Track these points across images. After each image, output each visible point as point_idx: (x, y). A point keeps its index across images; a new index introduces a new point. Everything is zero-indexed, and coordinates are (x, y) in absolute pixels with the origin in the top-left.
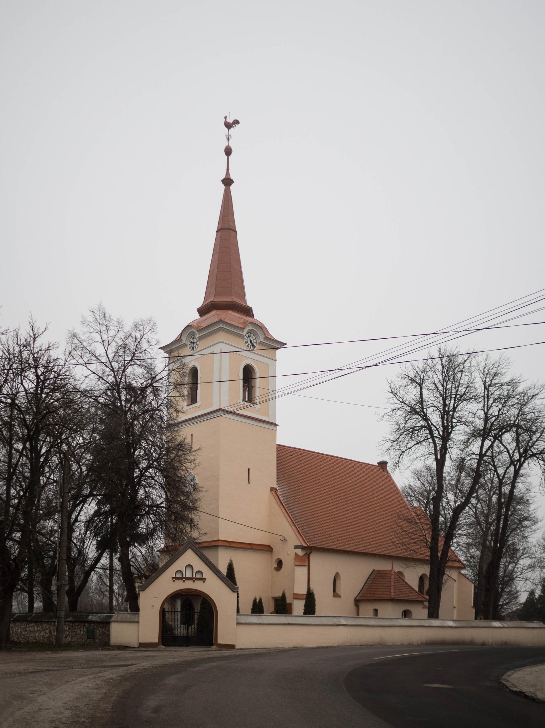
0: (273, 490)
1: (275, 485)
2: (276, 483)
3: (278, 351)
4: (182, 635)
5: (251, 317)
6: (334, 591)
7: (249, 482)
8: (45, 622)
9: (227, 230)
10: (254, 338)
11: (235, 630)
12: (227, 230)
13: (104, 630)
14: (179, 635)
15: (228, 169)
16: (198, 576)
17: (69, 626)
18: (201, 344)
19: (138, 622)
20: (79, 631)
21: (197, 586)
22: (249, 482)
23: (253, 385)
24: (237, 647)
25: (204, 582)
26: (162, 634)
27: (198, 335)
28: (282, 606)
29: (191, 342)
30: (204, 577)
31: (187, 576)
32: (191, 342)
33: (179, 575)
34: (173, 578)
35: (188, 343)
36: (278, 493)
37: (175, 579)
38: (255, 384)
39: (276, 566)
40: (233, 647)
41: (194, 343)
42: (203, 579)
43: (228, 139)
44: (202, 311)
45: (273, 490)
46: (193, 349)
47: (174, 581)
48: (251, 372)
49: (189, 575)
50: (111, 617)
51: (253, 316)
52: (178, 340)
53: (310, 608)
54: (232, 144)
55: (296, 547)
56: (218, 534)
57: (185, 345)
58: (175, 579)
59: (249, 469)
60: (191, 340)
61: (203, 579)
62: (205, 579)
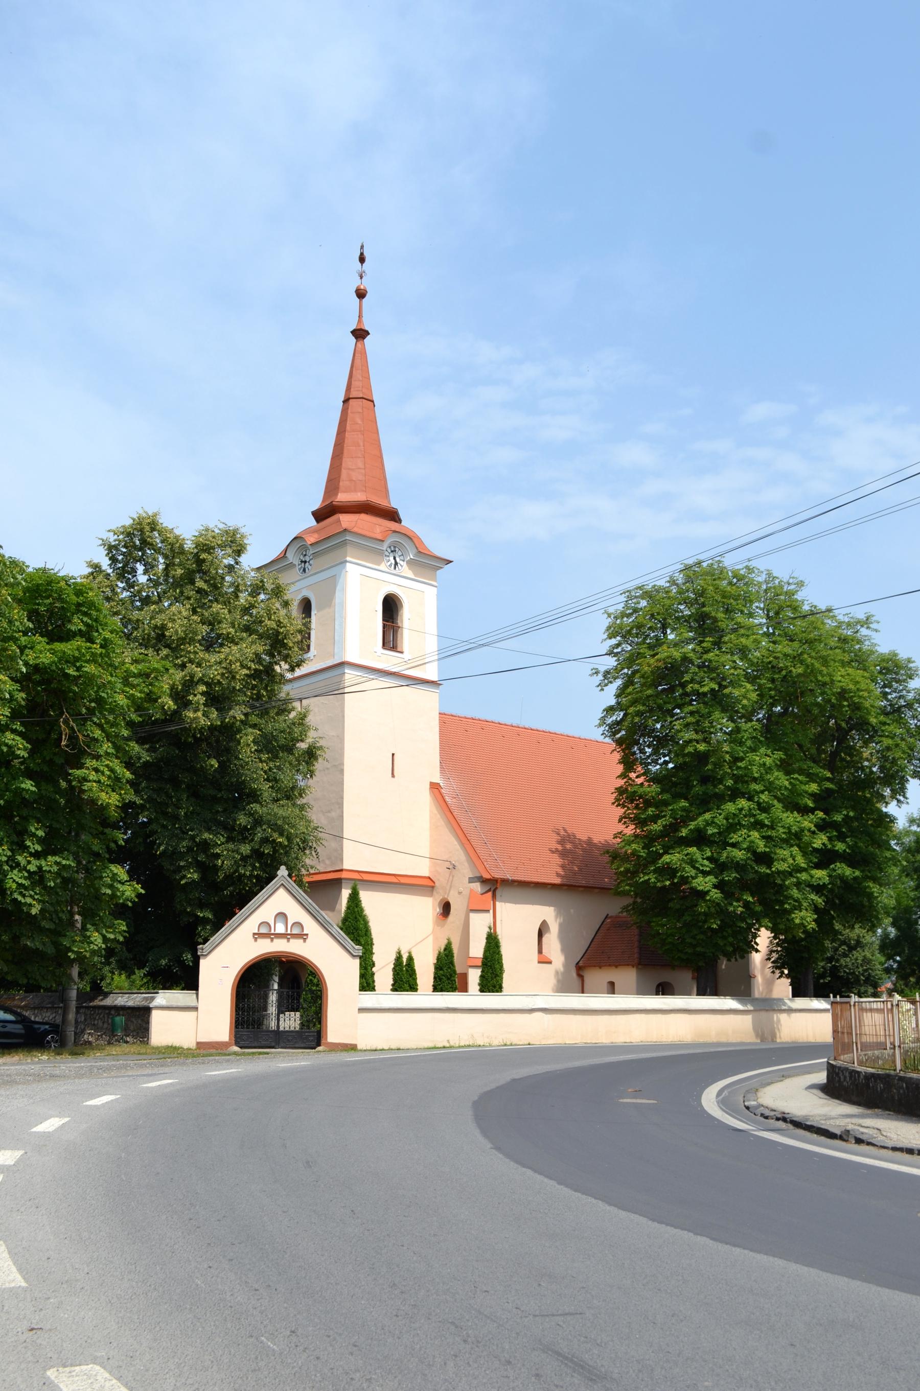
0: (434, 786)
1: (437, 779)
2: (438, 774)
3: (438, 572)
4: (292, 1029)
5: (396, 521)
6: (540, 951)
7: (393, 776)
8: (47, 1008)
9: (357, 399)
10: (400, 553)
11: (355, 1017)
12: (357, 399)
13: (140, 1021)
14: (287, 1029)
15: (360, 316)
16: (295, 931)
17: (86, 1015)
18: (315, 565)
19: (195, 1009)
20: (100, 1024)
21: (294, 947)
22: (393, 776)
23: (400, 624)
24: (359, 1047)
25: (305, 940)
26: (236, 1027)
27: (311, 551)
28: (447, 977)
29: (302, 562)
30: (305, 932)
31: (277, 932)
32: (302, 562)
33: (264, 930)
34: (254, 934)
35: (297, 562)
36: (443, 791)
37: (257, 936)
38: (402, 622)
39: (438, 910)
40: (353, 1048)
41: (305, 562)
42: (303, 936)
43: (361, 278)
44: (320, 515)
45: (434, 786)
46: (304, 570)
47: (256, 939)
48: (396, 604)
49: (280, 928)
50: (153, 999)
51: (398, 520)
52: (283, 556)
53: (492, 980)
54: (365, 284)
55: (471, 880)
56: (342, 860)
57: (292, 565)
58: (257, 936)
59: (393, 755)
60: (302, 557)
61: (303, 936)
62: (307, 935)
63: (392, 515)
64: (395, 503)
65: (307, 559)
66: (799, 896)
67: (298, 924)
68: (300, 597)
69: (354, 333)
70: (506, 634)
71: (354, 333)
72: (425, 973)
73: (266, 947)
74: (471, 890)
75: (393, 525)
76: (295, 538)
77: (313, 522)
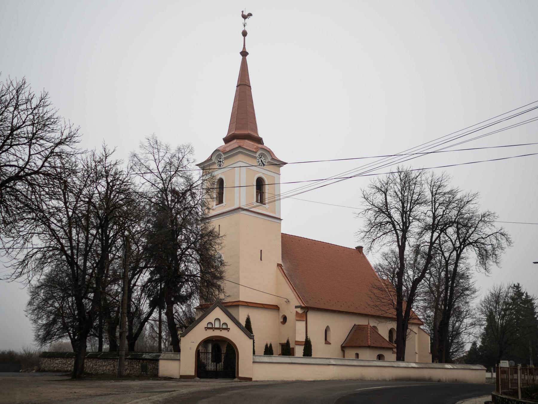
0: (279, 265)
1: (280, 262)
6: (326, 339)
7: (261, 260)
11: (254, 368)
16: (224, 327)
18: (226, 163)
19: (179, 360)
20: (135, 366)
22: (261, 260)
24: (253, 380)
27: (223, 156)
28: (287, 350)
33: (210, 326)
34: (205, 328)
35: (216, 162)
37: (207, 328)
39: (282, 320)
40: (250, 379)
42: (227, 329)
44: (227, 140)
45: (279, 265)
46: (220, 166)
49: (217, 326)
52: (210, 159)
53: (308, 352)
57: (214, 163)
58: (207, 328)
61: (227, 329)
63: (259, 141)
64: (260, 135)
65: (221, 160)
66: (164, 337)
67: (225, 324)
68: (218, 177)
69: (241, 53)
70: (422, 150)
71: (241, 53)
72: (277, 349)
73: (211, 333)
74: (297, 312)
75: (260, 146)
76: (216, 150)
77: (223, 143)
